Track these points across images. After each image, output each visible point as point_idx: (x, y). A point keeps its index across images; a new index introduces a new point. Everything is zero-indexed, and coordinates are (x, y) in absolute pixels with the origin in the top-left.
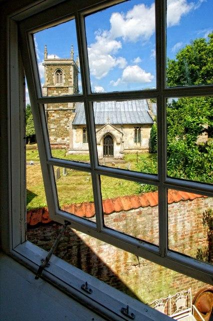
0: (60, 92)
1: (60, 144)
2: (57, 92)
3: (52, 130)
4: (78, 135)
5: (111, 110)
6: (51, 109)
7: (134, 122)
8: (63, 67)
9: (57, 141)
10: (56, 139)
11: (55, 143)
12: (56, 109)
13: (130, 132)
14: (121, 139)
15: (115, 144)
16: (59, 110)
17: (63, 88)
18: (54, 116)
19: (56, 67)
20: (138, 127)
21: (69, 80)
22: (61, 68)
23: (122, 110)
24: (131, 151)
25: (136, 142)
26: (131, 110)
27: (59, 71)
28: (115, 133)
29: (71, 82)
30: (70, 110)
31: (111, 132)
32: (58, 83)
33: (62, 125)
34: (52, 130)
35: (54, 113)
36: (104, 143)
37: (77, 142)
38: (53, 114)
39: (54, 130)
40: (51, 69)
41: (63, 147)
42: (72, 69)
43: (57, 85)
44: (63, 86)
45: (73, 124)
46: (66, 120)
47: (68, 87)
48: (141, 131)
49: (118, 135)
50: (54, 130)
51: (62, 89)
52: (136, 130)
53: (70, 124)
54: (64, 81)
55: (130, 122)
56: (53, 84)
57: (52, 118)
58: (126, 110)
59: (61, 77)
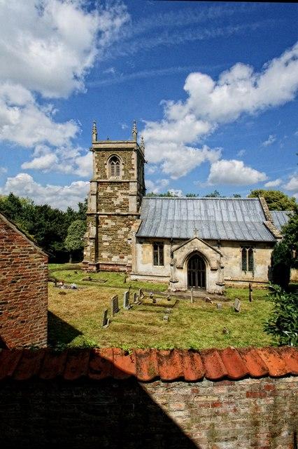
1: (117, 265)
2: (112, 188)
3: (105, 244)
5: (199, 218)
6: (103, 212)
7: (240, 237)
8: (120, 152)
10: (110, 257)
11: (109, 263)
13: (234, 254)
14: (219, 263)
15: (208, 269)
16: (115, 215)
17: (121, 183)
18: (107, 224)
19: (110, 154)
20: (247, 247)
21: (131, 172)
23: (218, 219)
26: (233, 219)
28: (208, 251)
29: (133, 175)
30: (132, 215)
31: (201, 250)
32: (113, 175)
34: (105, 244)
35: (107, 218)
36: (189, 267)
38: (106, 221)
41: (122, 269)
42: (134, 155)
43: (111, 179)
44: (120, 179)
45: (138, 235)
47: (128, 182)
48: (254, 254)
53: (133, 236)
54: (122, 173)
55: (232, 237)
57: (104, 226)
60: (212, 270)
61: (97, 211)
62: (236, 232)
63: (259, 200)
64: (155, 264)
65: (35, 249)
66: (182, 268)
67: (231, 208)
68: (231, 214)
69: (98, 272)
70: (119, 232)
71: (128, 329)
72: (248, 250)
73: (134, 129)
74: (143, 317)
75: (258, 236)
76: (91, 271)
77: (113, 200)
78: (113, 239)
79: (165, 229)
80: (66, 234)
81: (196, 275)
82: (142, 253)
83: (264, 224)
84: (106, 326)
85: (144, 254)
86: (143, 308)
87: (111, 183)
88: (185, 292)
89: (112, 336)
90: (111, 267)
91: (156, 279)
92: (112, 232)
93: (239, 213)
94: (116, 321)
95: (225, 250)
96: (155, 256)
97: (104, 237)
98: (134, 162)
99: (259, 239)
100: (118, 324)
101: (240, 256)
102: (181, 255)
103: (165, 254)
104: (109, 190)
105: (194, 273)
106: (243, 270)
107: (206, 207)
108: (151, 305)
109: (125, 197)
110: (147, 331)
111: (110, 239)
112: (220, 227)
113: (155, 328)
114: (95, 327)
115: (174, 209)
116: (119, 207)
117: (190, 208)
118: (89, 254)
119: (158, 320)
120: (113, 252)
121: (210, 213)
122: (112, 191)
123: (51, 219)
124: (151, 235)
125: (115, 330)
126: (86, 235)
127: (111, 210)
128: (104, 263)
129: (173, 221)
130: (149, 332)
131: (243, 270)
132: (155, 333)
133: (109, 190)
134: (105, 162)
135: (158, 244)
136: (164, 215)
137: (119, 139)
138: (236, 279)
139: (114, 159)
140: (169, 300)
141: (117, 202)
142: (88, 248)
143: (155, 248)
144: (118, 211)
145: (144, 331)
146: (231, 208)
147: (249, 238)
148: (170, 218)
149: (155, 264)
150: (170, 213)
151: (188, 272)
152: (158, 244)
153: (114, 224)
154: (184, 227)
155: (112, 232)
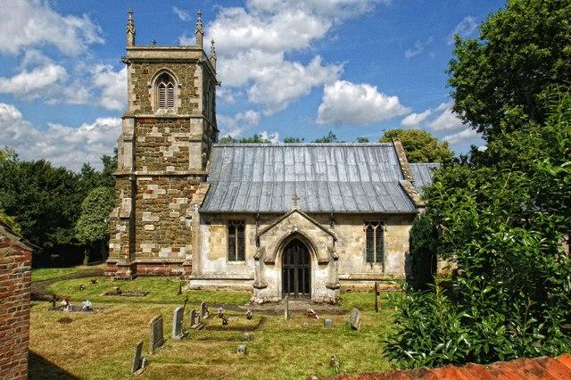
1: (167, 264)
2: (161, 130)
4: (214, 240)
6: (145, 171)
7: (364, 208)
9: (160, 254)
10: (156, 251)
12: (156, 173)
13: (355, 235)
14: (331, 251)
15: (314, 263)
16: (166, 176)
17: (175, 119)
18: (151, 192)
20: (375, 222)
21: (193, 101)
23: (332, 179)
24: (357, 285)
25: (369, 260)
27: (165, 77)
28: (314, 233)
29: (196, 105)
30: (195, 176)
31: (304, 231)
32: (162, 106)
33: (174, 214)
35: (151, 183)
36: (284, 261)
38: (150, 187)
39: (151, 227)
40: (145, 72)
42: (199, 72)
43: (159, 112)
44: (175, 113)
45: (202, 210)
47: (188, 119)
48: (385, 234)
54: (178, 103)
55: (352, 207)
56: (149, 109)
57: (146, 196)
61: (135, 168)
64: (231, 258)
65: (180, 97)
66: (273, 263)
67: (352, 162)
69: (134, 278)
70: (171, 205)
75: (391, 205)
76: (122, 278)
77: (162, 149)
78: (162, 218)
82: (210, 240)
85: (213, 240)
86: (207, 334)
88: (278, 303)
90: (157, 269)
91: (231, 284)
93: (363, 168)
95: (342, 230)
97: (146, 216)
98: (198, 83)
99: (393, 210)
101: (363, 239)
104: (155, 132)
105: (292, 271)
106: (368, 261)
108: (219, 328)
109: (183, 144)
110: (208, 373)
111: (157, 218)
112: (334, 191)
116: (172, 161)
117: (289, 161)
118: (118, 247)
119: (229, 353)
121: (320, 169)
122: (160, 135)
123: (51, 186)
124: (225, 208)
126: (115, 213)
127: (159, 167)
128: (146, 260)
129: (261, 183)
131: (368, 261)
133: (155, 132)
134: (149, 83)
135: (235, 223)
140: (249, 318)
141: (168, 154)
142: (118, 237)
143: (231, 231)
144: (170, 169)
146: (352, 162)
147: (377, 208)
148: (256, 179)
149: (231, 258)
150: (256, 172)
152: (235, 223)
153: (163, 192)
154: (278, 193)
155: (159, 205)
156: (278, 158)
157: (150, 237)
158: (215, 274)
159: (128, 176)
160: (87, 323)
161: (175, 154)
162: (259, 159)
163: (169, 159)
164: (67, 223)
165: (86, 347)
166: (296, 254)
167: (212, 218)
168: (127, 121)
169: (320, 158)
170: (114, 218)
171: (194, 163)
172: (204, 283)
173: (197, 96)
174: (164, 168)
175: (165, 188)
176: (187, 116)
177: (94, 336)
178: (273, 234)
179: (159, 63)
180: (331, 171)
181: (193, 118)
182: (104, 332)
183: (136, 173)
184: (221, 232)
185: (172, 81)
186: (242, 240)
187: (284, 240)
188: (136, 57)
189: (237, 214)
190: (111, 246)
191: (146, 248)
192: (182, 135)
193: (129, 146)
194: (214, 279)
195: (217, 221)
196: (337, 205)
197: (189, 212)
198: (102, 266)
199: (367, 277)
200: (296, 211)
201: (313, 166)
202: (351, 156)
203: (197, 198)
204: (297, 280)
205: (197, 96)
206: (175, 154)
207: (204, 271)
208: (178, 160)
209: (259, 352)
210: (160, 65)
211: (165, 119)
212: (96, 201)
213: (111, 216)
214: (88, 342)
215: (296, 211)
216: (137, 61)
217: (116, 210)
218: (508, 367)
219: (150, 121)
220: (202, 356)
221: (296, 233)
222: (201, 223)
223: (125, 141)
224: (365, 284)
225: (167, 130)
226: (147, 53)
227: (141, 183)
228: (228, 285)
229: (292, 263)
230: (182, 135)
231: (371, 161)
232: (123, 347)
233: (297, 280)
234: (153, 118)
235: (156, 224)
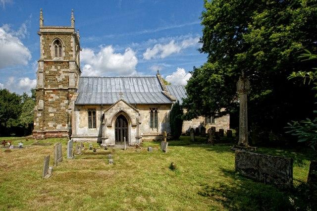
0: (59, 67)
1: (60, 132)
2: (56, 67)
3: (51, 115)
4: (82, 118)
5: (119, 91)
6: (49, 88)
7: (149, 102)
8: (62, 36)
9: (57, 128)
10: (55, 126)
11: (54, 130)
12: (54, 88)
13: (145, 115)
14: (137, 120)
15: (130, 126)
16: (59, 90)
17: (62, 62)
18: (52, 98)
19: (53, 37)
20: (154, 108)
21: (70, 53)
22: (61, 38)
23: (132, 91)
24: (146, 138)
25: (152, 127)
26: (142, 91)
27: (57, 42)
28: (130, 111)
29: (72, 56)
30: (72, 89)
31: (125, 110)
32: (56, 56)
33: (62, 108)
34: (51, 115)
35: (52, 93)
36: (116, 125)
37: (81, 127)
38: (52, 95)
39: (53, 115)
40: (48, 39)
41: (64, 135)
42: (73, 40)
43: (55, 59)
44: (62, 60)
45: (76, 103)
46: (66, 102)
47: (68, 62)
48: (158, 114)
49: (134, 114)
50: (53, 115)
51: (62, 65)
52: (152, 112)
53: (72, 106)
54: (64, 54)
55: (144, 102)
56: (50, 57)
57: (50, 100)
58: (137, 91)
59: (60, 50)
60: (133, 126)
61: (45, 86)
62: (145, 98)
63: (157, 77)
64: (90, 127)
66: (111, 127)
67: (140, 83)
68: (140, 87)
69: (45, 139)
71: (74, 177)
72: (154, 111)
73: (73, 17)
74: (89, 163)
75: (160, 100)
76: (40, 139)
78: (57, 111)
79: (96, 98)
80: (19, 113)
81: (121, 132)
83: (162, 93)
84: (48, 176)
85: (81, 119)
86: (86, 156)
87: (55, 62)
88: (113, 146)
89: (54, 186)
91: (90, 139)
92: (56, 104)
93: (145, 86)
94: (61, 169)
95: (141, 112)
96: (90, 121)
97: (50, 110)
98: (73, 44)
99: (162, 102)
100: (62, 172)
101: (149, 117)
102: (110, 116)
103: (97, 118)
104: (53, 69)
105: (120, 130)
106: (151, 127)
107: (124, 83)
108: (92, 154)
109: (66, 75)
110: (96, 175)
111: (55, 110)
112: (134, 96)
113: (105, 172)
114: (34, 178)
115: (102, 85)
116: (61, 83)
117: (113, 84)
118: (38, 124)
119: (104, 164)
120: (57, 121)
121: (127, 87)
122: (56, 70)
123: (9, 101)
124: (86, 102)
125: (59, 179)
126: (36, 108)
127: (55, 85)
128: (51, 131)
129: (101, 93)
130: (99, 177)
131: (151, 127)
132: (105, 177)
133: (53, 69)
135: (91, 110)
136: (95, 89)
137: (61, 25)
138: (147, 135)
139: (57, 42)
140: (106, 149)
141: (60, 79)
142: (38, 120)
143: (90, 114)
144: (61, 87)
145: (92, 176)
146: (140, 83)
147: (155, 102)
148: (99, 91)
149: (90, 127)
150: (99, 88)
151: (115, 130)
152: (91, 110)
154: (110, 96)
155: (56, 104)
156: (108, 82)
157: (52, 120)
158: (82, 135)
159: (41, 89)
160: (19, 153)
161: (63, 79)
162: (100, 83)
163: (60, 82)
164: (15, 117)
165: (15, 163)
166: (122, 120)
167: (81, 107)
168: (40, 63)
169: (127, 82)
170: (36, 111)
171: (72, 83)
172: (77, 139)
173: (72, 51)
174: (58, 86)
175: (59, 96)
176: (68, 61)
177: (22, 158)
178: (111, 112)
179: (54, 35)
180: (132, 88)
181: (71, 61)
182: (28, 156)
183: (45, 88)
184: (85, 114)
185: (61, 43)
186: (95, 118)
187: (116, 115)
188: (44, 31)
189: (93, 105)
190: (35, 124)
191: (51, 124)
192: (66, 70)
193: (42, 75)
194: (83, 137)
195: (83, 109)
196: (137, 101)
197: (70, 107)
198: (31, 136)
199: (151, 135)
200: (121, 100)
201: (124, 85)
202: (139, 81)
203: (73, 98)
204: (122, 135)
205: (72, 51)
206: (63, 79)
207: (77, 133)
208: (64, 82)
209: (121, 163)
210: (55, 36)
211: (58, 62)
212: (28, 106)
213: (34, 109)
214: (18, 160)
215: (121, 100)
216: (45, 34)
217: (36, 107)
218: (14, 209)
219: (51, 63)
220: (88, 166)
221: (121, 111)
222: (75, 110)
223: (40, 72)
224: (149, 138)
225: (59, 67)
226: (49, 30)
227: (48, 93)
228: (89, 140)
229: (120, 127)
230: (66, 70)
231: (148, 83)
232: (39, 163)
233: (122, 135)
234: (52, 62)
235: (55, 113)
